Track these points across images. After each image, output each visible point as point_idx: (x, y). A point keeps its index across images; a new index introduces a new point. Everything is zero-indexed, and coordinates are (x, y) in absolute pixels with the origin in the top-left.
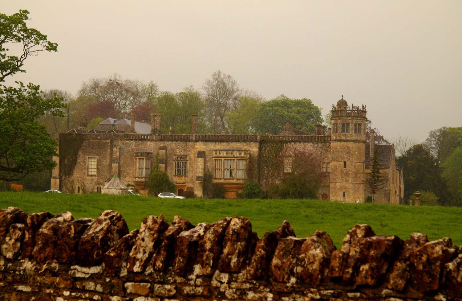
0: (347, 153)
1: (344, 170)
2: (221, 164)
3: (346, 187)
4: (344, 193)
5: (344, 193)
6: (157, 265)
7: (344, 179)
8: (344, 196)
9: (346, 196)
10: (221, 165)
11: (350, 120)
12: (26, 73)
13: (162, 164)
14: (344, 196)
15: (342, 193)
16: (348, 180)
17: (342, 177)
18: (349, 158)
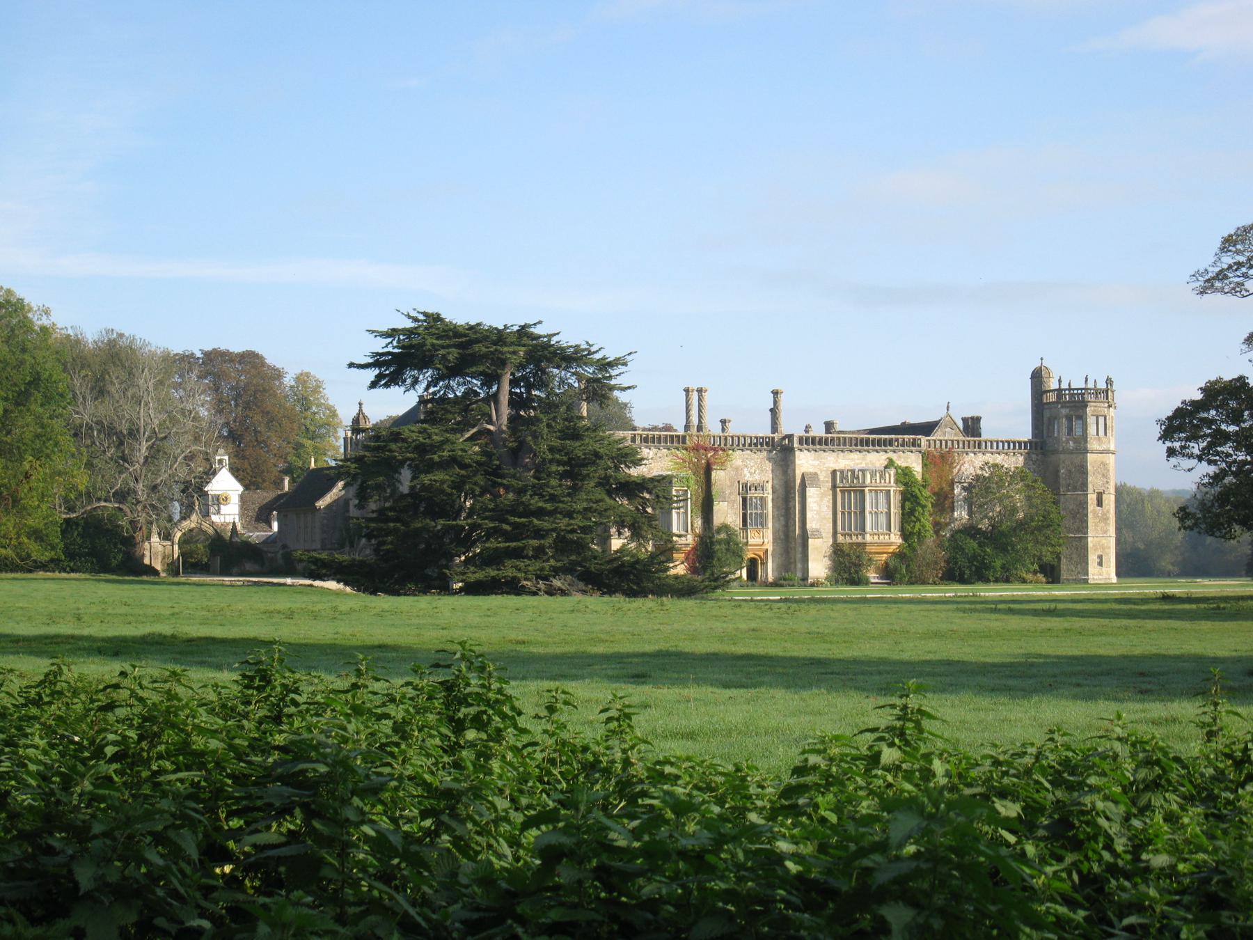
0: (1103, 475)
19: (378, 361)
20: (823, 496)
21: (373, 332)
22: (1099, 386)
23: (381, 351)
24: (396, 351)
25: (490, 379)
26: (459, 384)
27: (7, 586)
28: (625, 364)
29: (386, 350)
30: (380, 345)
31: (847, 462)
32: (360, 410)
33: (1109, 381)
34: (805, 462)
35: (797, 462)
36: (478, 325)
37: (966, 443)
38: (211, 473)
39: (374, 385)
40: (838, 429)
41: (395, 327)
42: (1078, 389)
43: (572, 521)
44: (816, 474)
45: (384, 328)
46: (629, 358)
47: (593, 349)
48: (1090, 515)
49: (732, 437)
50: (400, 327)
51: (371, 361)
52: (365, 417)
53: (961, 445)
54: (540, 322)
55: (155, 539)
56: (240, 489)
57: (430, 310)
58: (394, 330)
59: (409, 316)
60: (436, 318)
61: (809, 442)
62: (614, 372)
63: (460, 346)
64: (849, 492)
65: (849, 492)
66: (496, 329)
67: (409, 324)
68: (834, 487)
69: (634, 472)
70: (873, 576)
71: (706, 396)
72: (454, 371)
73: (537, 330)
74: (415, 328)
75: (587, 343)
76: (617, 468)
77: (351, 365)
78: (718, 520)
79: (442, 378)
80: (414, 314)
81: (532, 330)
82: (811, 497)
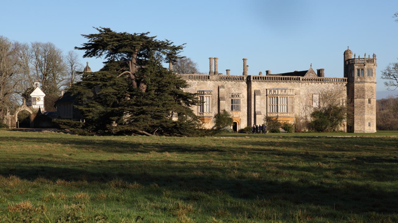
0: (371, 92)
2: (284, 100)
3: (371, 118)
6: (110, 166)
7: (369, 112)
10: (284, 102)
12: (173, 43)
13: (223, 101)
14: (369, 126)
16: (372, 113)
17: (368, 111)
18: (373, 95)
19: (87, 47)
20: (261, 99)
21: (84, 35)
22: (370, 57)
23: (87, 43)
24: (93, 43)
25: (130, 54)
26: (119, 56)
27: (1, 131)
28: (182, 49)
29: (89, 43)
30: (87, 41)
31: (271, 86)
32: (87, 65)
33: (374, 56)
34: (255, 86)
35: (252, 86)
36: (125, 33)
37: (276, 78)
38: (32, 90)
39: (85, 56)
40: (271, 74)
41: (92, 34)
42: (362, 59)
43: (158, 108)
44: (259, 90)
45: (88, 34)
46: (183, 46)
47: (170, 43)
48: (366, 107)
49: (332, 79)
50: (94, 34)
51: (84, 46)
52: (89, 68)
53: (336, 80)
54: (149, 33)
55: (8, 114)
56: (45, 95)
57: (106, 27)
58: (92, 35)
59: (97, 29)
60: (108, 30)
61: (256, 78)
62: (177, 52)
63: (118, 41)
64: (282, 97)
65: (282, 97)
66: (131, 35)
67: (98, 33)
68: (267, 95)
69: (185, 90)
70: (281, 130)
71: (218, 61)
72: (115, 51)
73: (149, 36)
74: (100, 34)
75: (167, 40)
76: (178, 88)
77: (76, 48)
78: (222, 108)
79: (111, 54)
80: (100, 29)
81: (146, 35)
82: (257, 99)
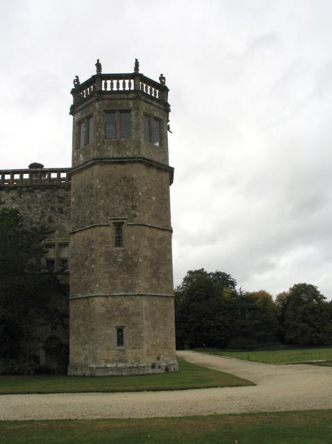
0: (126, 196)
1: (118, 252)
3: (126, 309)
4: (120, 330)
5: (120, 330)
7: (118, 281)
8: (120, 341)
9: (126, 341)
11: (131, 102)
14: (120, 341)
15: (113, 332)
16: (131, 287)
18: (133, 212)
